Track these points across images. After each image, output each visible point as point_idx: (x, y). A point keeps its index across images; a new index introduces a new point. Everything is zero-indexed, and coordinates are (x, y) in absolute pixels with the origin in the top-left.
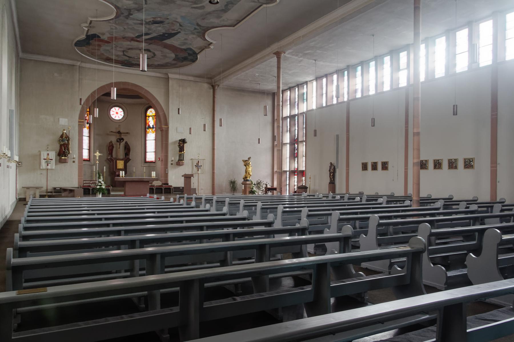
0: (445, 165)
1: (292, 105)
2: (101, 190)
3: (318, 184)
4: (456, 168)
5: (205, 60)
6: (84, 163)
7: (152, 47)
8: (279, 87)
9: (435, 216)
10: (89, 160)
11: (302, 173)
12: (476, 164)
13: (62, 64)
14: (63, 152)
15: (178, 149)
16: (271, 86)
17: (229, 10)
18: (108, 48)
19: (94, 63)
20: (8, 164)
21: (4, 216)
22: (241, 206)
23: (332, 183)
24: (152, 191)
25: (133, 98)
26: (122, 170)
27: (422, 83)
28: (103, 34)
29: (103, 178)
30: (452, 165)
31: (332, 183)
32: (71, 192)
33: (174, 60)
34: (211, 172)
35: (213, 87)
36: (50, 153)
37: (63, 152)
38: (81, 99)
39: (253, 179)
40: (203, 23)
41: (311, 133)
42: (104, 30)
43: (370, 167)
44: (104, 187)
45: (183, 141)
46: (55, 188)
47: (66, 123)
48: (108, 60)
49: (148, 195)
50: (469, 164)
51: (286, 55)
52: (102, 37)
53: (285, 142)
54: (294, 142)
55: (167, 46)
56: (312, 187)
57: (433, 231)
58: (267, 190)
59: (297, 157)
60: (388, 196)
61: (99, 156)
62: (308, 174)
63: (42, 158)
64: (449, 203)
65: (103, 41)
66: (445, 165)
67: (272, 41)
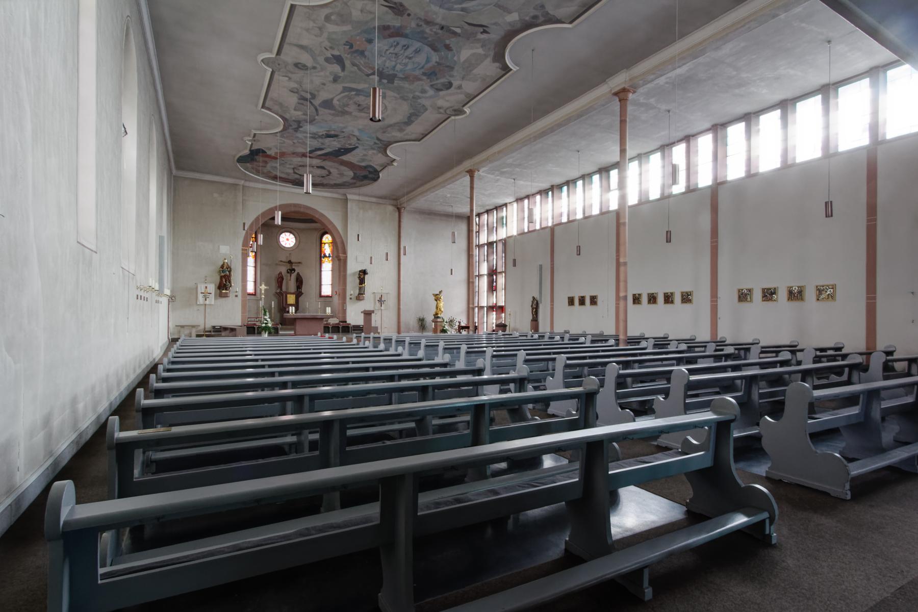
0: (661, 299)
1: (490, 230)
2: (266, 329)
3: (518, 322)
4: (672, 302)
5: (388, 179)
6: (249, 297)
7: (327, 164)
8: (472, 210)
9: (696, 363)
10: (255, 294)
11: (501, 309)
12: (695, 298)
13: (223, 184)
14: (224, 284)
15: (358, 281)
16: (465, 210)
17: (413, 122)
18: (274, 165)
19: (257, 181)
20: (157, 298)
21: (151, 359)
22: (440, 349)
23: (535, 320)
24: (327, 329)
25: (302, 220)
26: (292, 305)
27: (630, 207)
28: (270, 149)
29: (270, 314)
30: (668, 299)
31: (535, 320)
32: (232, 331)
33: (353, 178)
34: (396, 309)
35: (399, 210)
36: (208, 286)
37: (224, 284)
38: (244, 224)
39: (445, 316)
40: (385, 137)
41: (510, 263)
42: (271, 145)
43: (577, 301)
44: (270, 325)
45: (364, 272)
46: (214, 327)
47: (228, 250)
48: (275, 178)
49: (319, 334)
50: (686, 298)
51: (481, 173)
52: (269, 153)
53: (481, 273)
54: (492, 273)
55: (344, 163)
56: (512, 325)
57: (621, 372)
58: (461, 328)
59: (496, 290)
60: (593, 335)
61: (265, 290)
62: (508, 310)
63: (199, 291)
64: (662, 343)
65: (269, 156)
66: (645, 299)
67: (464, 158)
